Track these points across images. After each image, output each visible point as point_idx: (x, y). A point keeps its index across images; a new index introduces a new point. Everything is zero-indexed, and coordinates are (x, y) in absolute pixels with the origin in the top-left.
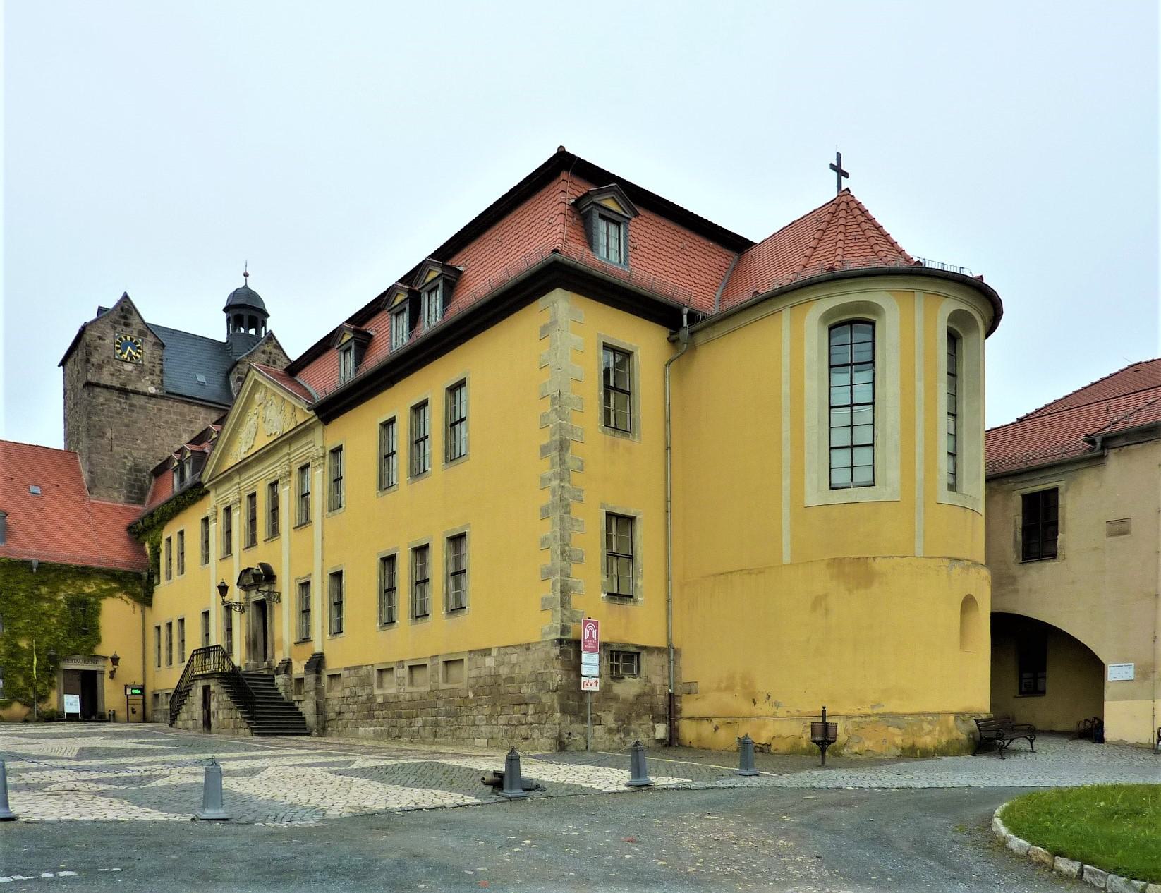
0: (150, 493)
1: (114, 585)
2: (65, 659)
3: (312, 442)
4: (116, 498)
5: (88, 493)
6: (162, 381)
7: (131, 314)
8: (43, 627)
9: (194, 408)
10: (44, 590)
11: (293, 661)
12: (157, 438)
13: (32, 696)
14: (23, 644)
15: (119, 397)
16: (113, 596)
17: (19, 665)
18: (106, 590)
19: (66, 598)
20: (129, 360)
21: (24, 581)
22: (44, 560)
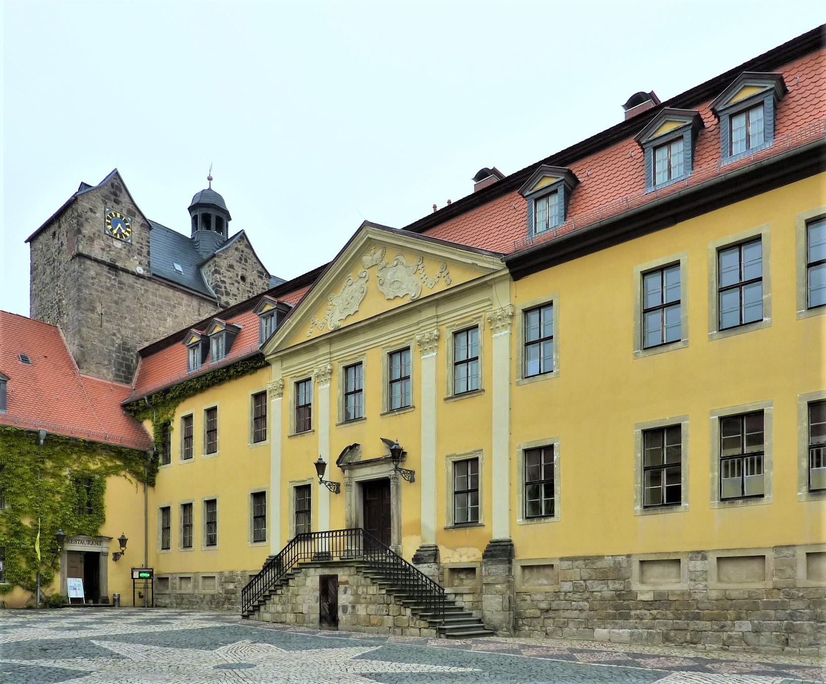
0: (137, 374)
1: (118, 463)
2: (69, 540)
3: (490, 300)
4: (106, 375)
5: (76, 366)
6: (149, 262)
7: (121, 192)
8: (48, 505)
9: (177, 293)
10: (49, 464)
11: (441, 549)
12: (144, 319)
13: (35, 580)
14: (27, 522)
15: (109, 273)
16: (117, 474)
17: (23, 546)
18: (111, 467)
19: (71, 474)
20: (118, 237)
21: (28, 452)
22: (51, 431)
